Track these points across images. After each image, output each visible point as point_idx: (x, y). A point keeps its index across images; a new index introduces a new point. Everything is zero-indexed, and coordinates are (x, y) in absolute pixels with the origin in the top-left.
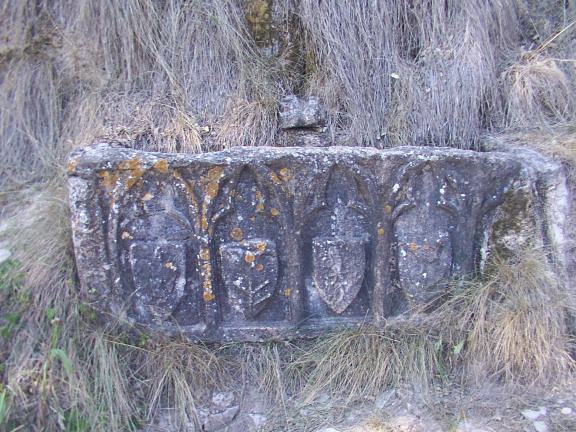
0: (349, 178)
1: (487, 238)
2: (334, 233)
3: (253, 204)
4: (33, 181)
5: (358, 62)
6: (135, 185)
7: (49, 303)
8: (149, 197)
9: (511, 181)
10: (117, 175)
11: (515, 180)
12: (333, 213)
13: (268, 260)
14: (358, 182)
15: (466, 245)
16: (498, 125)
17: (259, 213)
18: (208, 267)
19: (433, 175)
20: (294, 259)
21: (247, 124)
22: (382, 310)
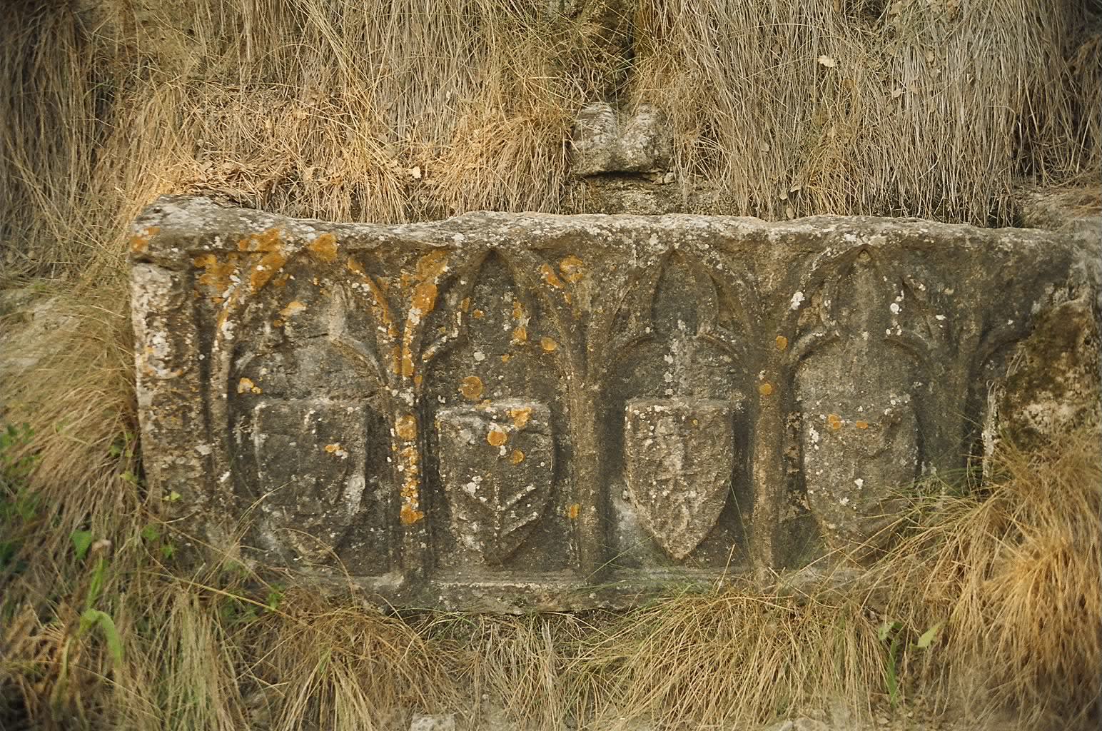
0: (700, 279)
1: (993, 409)
2: (669, 392)
3: (506, 328)
4: (32, 273)
5: (743, 31)
6: (269, 283)
7: (79, 520)
8: (296, 308)
9: (1049, 290)
10: (233, 263)
11: (1057, 287)
12: (668, 350)
13: (535, 444)
14: (720, 287)
15: (947, 419)
16: (1061, 167)
17: (518, 346)
18: (411, 453)
19: (876, 276)
20: (584, 438)
21: (502, 165)
22: (769, 554)
